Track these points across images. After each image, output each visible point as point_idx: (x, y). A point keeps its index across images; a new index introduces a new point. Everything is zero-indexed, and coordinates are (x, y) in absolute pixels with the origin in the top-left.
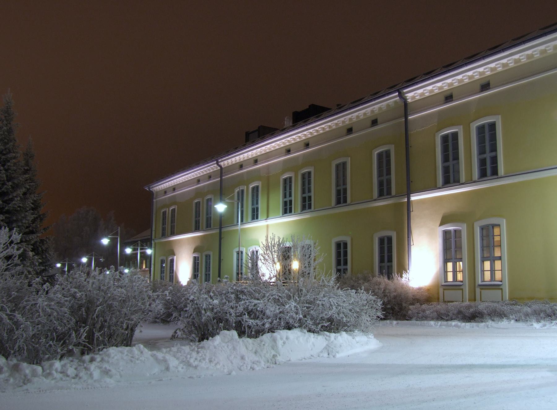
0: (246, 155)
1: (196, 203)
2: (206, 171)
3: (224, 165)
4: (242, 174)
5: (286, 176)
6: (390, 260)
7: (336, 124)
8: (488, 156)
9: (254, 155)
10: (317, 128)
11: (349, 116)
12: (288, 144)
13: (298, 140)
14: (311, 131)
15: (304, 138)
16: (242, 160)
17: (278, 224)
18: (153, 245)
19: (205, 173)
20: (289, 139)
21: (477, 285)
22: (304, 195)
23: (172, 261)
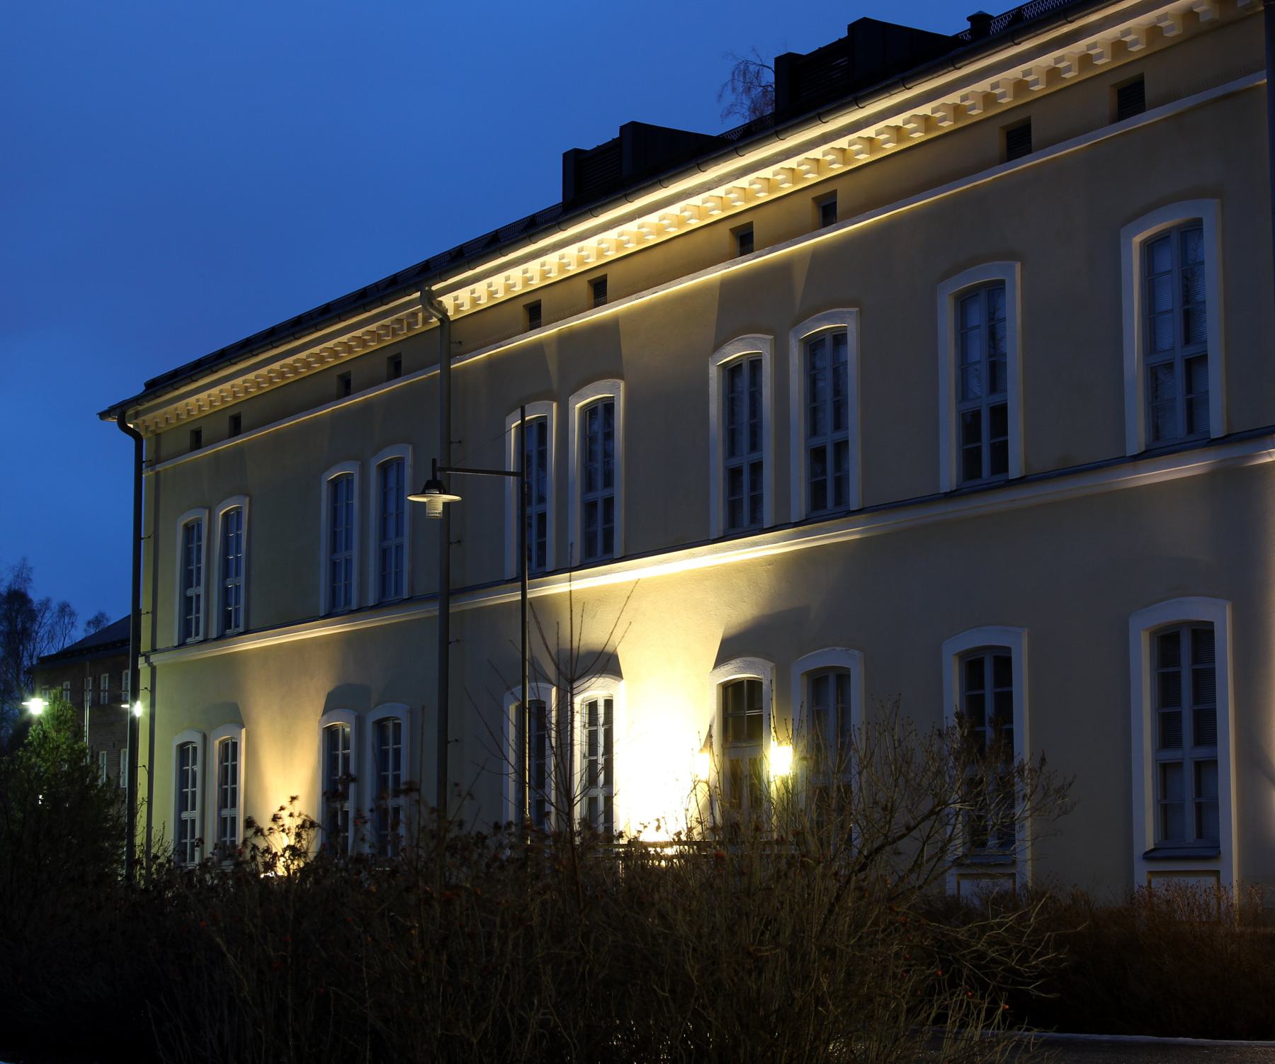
0: (534, 266)
1: (335, 483)
2: (362, 342)
3: (458, 308)
4: (538, 347)
5: (732, 353)
6: (1207, 730)
7: (957, 110)
8: (533, 510)
9: (593, 262)
10: (869, 132)
11: (1016, 72)
12: (741, 206)
13: (788, 188)
14: (842, 143)
15: (813, 178)
16: (536, 283)
17: (701, 578)
18: (144, 681)
19: (374, 346)
20: (744, 182)
21: (1138, 851)
22: (591, 496)
23: (230, 750)
